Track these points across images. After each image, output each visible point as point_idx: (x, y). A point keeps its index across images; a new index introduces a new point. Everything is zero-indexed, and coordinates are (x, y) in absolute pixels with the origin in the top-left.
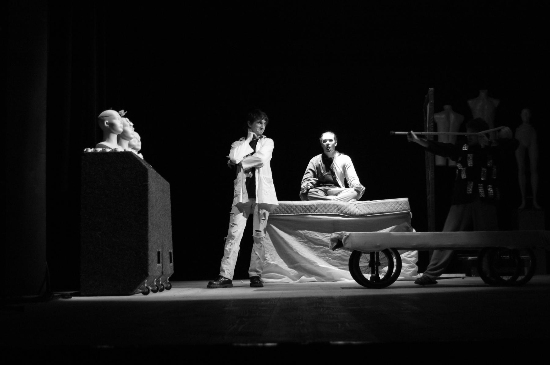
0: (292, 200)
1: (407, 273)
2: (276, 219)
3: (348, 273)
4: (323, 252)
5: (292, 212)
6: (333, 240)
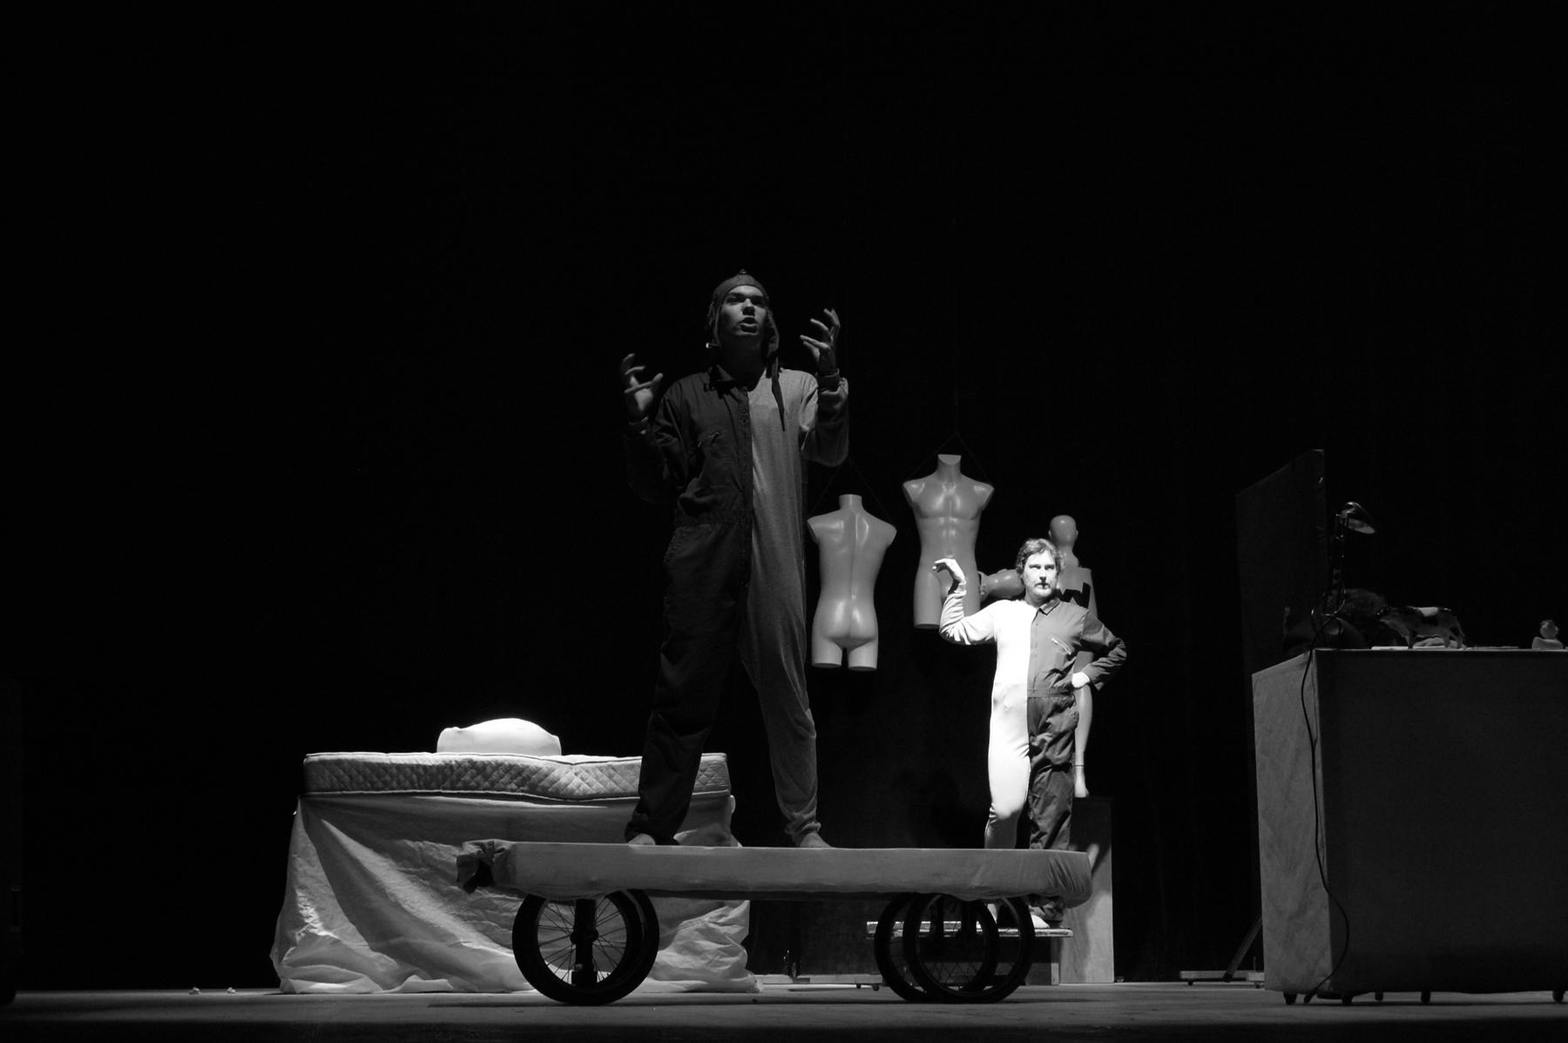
0: (387, 751)
1: (715, 970)
2: (332, 805)
3: (508, 956)
4: (472, 907)
5: (386, 785)
6: (464, 862)
